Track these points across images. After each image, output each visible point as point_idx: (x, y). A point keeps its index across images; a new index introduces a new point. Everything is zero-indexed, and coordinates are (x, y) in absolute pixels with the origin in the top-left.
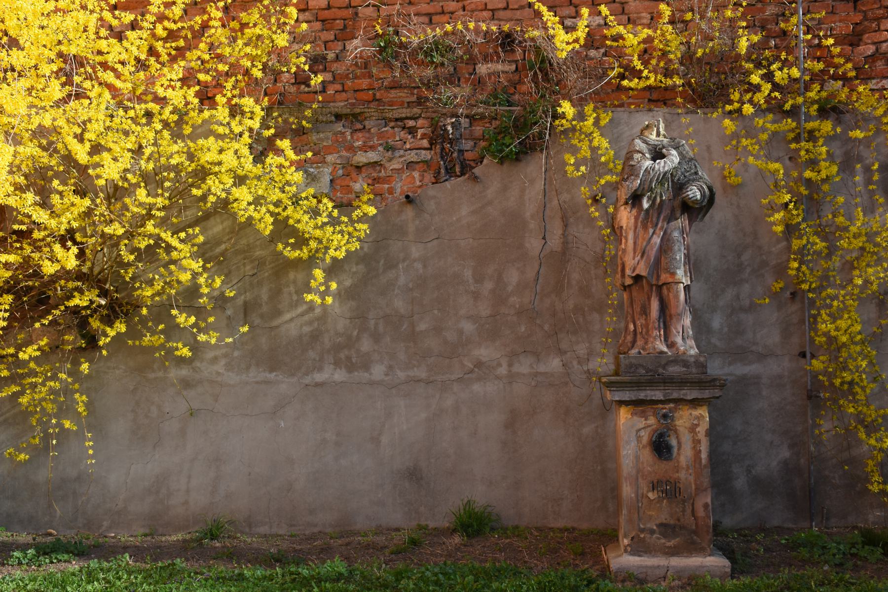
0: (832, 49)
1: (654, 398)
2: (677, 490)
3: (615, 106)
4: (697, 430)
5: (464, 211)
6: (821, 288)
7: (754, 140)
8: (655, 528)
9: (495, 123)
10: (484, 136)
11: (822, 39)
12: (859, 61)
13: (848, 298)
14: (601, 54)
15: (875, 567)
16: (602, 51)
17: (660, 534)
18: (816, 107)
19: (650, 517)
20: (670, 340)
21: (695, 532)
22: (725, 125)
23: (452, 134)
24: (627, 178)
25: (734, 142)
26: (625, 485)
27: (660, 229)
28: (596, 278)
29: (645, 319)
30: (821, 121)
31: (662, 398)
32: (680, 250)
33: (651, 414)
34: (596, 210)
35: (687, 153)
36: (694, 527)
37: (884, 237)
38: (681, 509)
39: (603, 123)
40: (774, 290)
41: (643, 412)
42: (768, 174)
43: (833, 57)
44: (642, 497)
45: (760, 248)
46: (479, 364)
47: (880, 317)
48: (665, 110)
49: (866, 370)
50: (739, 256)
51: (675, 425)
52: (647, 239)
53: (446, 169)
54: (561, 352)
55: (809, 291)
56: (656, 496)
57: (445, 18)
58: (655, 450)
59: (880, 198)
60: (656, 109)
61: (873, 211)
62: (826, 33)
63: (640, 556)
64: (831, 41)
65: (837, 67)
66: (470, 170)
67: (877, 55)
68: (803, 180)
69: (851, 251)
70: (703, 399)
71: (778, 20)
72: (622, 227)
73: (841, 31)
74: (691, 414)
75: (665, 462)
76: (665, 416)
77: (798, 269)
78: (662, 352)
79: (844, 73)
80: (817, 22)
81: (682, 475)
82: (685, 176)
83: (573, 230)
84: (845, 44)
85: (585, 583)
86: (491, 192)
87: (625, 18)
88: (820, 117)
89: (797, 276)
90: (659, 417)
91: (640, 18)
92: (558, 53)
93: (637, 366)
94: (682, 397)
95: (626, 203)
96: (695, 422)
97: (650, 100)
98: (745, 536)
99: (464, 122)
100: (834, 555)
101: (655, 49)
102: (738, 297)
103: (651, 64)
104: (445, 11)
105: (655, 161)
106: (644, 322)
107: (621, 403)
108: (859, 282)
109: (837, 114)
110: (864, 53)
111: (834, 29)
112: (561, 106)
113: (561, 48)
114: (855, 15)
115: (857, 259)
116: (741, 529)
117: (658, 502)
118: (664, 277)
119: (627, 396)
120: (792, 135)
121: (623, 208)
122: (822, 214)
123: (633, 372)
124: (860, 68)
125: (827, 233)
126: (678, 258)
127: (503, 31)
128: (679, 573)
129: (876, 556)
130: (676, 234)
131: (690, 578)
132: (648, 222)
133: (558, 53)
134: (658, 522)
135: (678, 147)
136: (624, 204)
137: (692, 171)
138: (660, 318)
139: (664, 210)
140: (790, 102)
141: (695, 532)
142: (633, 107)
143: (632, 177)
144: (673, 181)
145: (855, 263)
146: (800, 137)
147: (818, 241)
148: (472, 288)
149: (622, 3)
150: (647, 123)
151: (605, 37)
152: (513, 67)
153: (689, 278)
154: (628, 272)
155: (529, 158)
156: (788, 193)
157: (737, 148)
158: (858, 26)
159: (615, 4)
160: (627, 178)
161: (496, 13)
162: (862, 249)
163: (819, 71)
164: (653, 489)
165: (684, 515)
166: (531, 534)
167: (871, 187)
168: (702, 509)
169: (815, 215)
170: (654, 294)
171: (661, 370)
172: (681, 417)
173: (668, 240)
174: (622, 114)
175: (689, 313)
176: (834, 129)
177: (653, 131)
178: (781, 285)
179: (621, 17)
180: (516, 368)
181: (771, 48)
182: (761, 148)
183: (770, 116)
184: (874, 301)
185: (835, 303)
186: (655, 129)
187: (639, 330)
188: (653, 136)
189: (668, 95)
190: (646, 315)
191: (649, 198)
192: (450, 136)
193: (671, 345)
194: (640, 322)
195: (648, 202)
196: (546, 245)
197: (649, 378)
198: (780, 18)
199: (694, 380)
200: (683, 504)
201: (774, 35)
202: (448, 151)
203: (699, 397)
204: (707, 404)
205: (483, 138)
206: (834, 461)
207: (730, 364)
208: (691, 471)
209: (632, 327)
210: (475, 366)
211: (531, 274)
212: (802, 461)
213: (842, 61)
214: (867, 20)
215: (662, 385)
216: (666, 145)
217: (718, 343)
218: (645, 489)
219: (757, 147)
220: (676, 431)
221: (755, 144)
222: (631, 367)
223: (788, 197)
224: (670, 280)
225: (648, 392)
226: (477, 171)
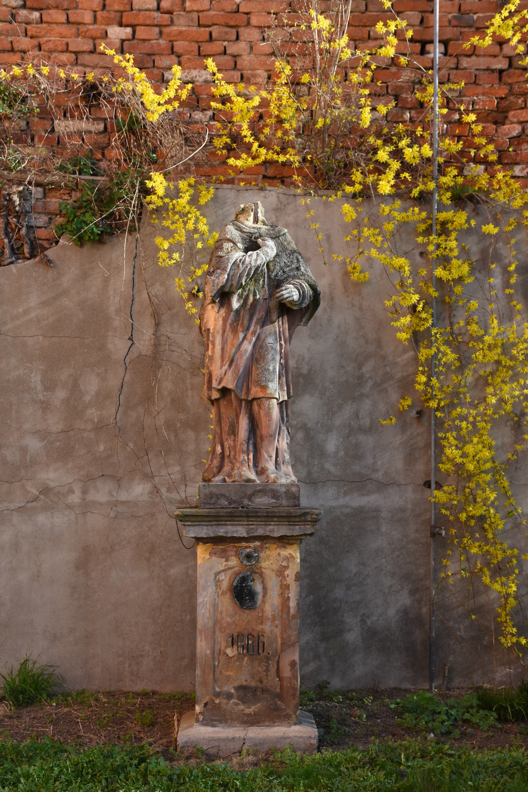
0: (473, 126)
1: (235, 535)
2: (261, 645)
3: (222, 183)
4: (286, 573)
5: (34, 301)
6: (452, 406)
7: (377, 231)
8: (233, 691)
9: (76, 195)
10: (61, 211)
11: (462, 114)
12: (503, 143)
13: (479, 419)
14: (208, 117)
15: (485, 735)
16: (210, 113)
17: (238, 699)
18: (449, 194)
19: (228, 678)
20: (260, 466)
21: (280, 696)
22: (344, 211)
23: (19, 205)
24: (213, 272)
25: (355, 232)
26: (199, 639)
27: (252, 334)
28: (192, 389)
29: (234, 440)
30: (455, 212)
31: (245, 535)
32: (274, 359)
33: (233, 553)
34: (194, 306)
35: (289, 243)
36: (278, 690)
37: (521, 350)
38: (264, 668)
39: (203, 201)
40: (401, 409)
41: (224, 551)
42: (392, 270)
43: (474, 136)
44: (219, 654)
45: (384, 358)
46: (46, 490)
47: (515, 442)
48: (281, 189)
49: (496, 503)
50: (360, 367)
51: (261, 567)
52: (236, 345)
53: (12, 248)
54: (148, 477)
55: (437, 409)
56: (236, 652)
57: (16, 58)
58: (236, 597)
59: (517, 304)
60: (268, 188)
61: (511, 319)
62: (468, 107)
63: (213, 726)
64: (472, 117)
65: (478, 148)
66: (42, 252)
67: (523, 137)
68: (434, 279)
69: (485, 365)
70: (293, 536)
71: (414, 89)
72: (209, 330)
73: (484, 106)
74: (279, 554)
75: (247, 611)
76: (249, 557)
77: (427, 384)
78: (249, 480)
79: (486, 156)
80: (457, 94)
81: (267, 627)
82: (284, 272)
83: (166, 329)
84: (488, 122)
85: (136, 762)
86: (66, 281)
87: (237, 75)
88: (456, 206)
89: (425, 392)
90: (241, 558)
91: (255, 76)
92: (149, 114)
93: (219, 496)
94: (268, 534)
95: (213, 302)
96: (284, 564)
97: (265, 177)
98: (351, 699)
99: (37, 192)
100: (443, 722)
101: (270, 116)
102: (356, 415)
103: (263, 133)
104: (16, 49)
105: (246, 253)
106: (232, 443)
107: (199, 540)
108: (493, 400)
109: (474, 204)
110: (508, 134)
111: (477, 104)
112: (150, 179)
113: (152, 109)
114: (499, 88)
115: (492, 374)
116: (349, 691)
117: (237, 660)
118: (255, 392)
119: (204, 532)
120: (422, 227)
121: (210, 307)
122: (454, 320)
123: (213, 504)
124: (504, 151)
125: (459, 342)
126: (271, 368)
127: (87, 81)
128: (257, 744)
129: (488, 722)
130: (270, 340)
131: (270, 752)
132: (238, 325)
133: (149, 114)
134: (236, 684)
135: (278, 237)
136: (211, 303)
137: (293, 266)
138: (249, 439)
139: (257, 312)
140: (421, 187)
141: (280, 696)
142: (242, 184)
143: (219, 271)
144: (269, 277)
145: (490, 378)
146: (432, 229)
147: (448, 351)
148: (41, 397)
149: (235, 56)
150: (242, 206)
151: (213, 97)
152: (101, 127)
153: (285, 393)
154: (215, 384)
155: (115, 240)
156: (416, 292)
157: (359, 240)
158: (503, 101)
159: (225, 57)
160: (213, 272)
161: (80, 57)
162: (498, 362)
163: (457, 152)
164: (233, 645)
165: (267, 675)
166: (97, 700)
167: (507, 291)
168: (289, 668)
169: (447, 321)
170: (243, 411)
171: (246, 502)
172: (268, 557)
173: (261, 347)
174: (228, 192)
175: (286, 432)
176: (468, 221)
177: (249, 216)
178: (409, 402)
179: (232, 73)
180: (93, 496)
181: (406, 121)
182: (385, 239)
183: (398, 203)
184: (508, 423)
186: (252, 214)
187: (227, 453)
188: (250, 223)
189: (285, 172)
190: (235, 436)
191: (240, 297)
192: (17, 209)
193: (261, 472)
195: (238, 300)
196: (134, 346)
197: (230, 510)
198: (417, 86)
199: (282, 514)
200: (267, 662)
201: (409, 106)
202: (14, 226)
203: (288, 534)
204: (298, 542)
205: (60, 214)
206: (460, 610)
207: (346, 494)
208: (277, 622)
209: (219, 449)
210: (40, 493)
211: (114, 382)
212: (424, 610)
213: (484, 141)
214: (513, 95)
215: (245, 519)
216: (263, 234)
217: (332, 469)
218: (223, 644)
219: (380, 238)
220: (261, 575)
221: (378, 235)
222: (211, 498)
223: (415, 298)
224: (261, 395)
225: (229, 527)
226: (51, 253)
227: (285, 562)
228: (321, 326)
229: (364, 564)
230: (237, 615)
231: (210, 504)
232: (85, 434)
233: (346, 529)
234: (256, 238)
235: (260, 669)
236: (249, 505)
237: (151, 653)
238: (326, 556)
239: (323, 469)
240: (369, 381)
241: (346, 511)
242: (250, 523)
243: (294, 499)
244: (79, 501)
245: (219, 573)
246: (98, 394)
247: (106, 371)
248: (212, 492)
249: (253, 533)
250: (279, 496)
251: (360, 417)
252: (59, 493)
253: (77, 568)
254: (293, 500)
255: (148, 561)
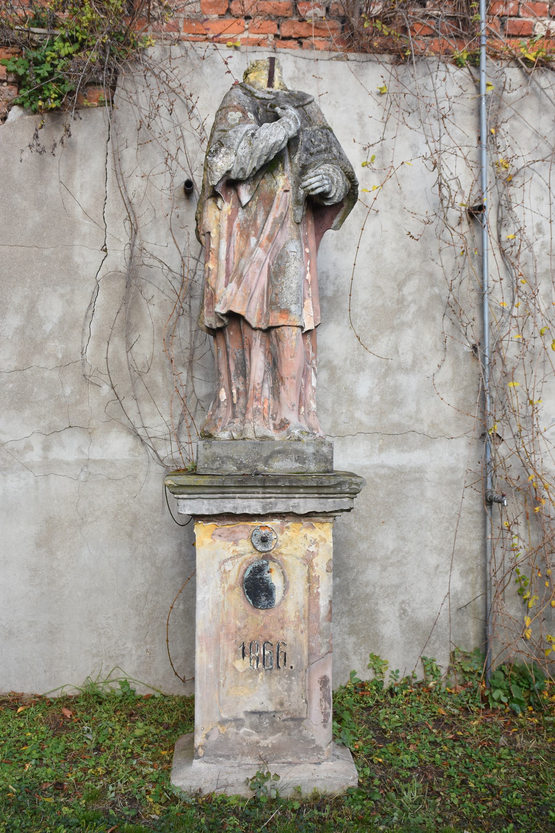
17: (251, 728)
24: (216, 151)
33: (246, 536)
38: (286, 686)
50: (400, 286)
74: (305, 536)
78: (264, 438)
94: (291, 510)
96: (313, 549)
123: (217, 469)
164: (244, 656)
165: (289, 696)
171: (261, 467)
180: (57, 453)
185: (147, 521)
194: (238, 384)
200: (289, 678)
203: (318, 511)
207: (381, 450)
215: (260, 490)
217: (365, 419)
218: (231, 655)
222: (214, 461)
225: (239, 501)
227: (313, 546)
228: (351, 233)
229: (403, 539)
230: (250, 618)
231: (212, 469)
232: (46, 374)
233: (381, 495)
234: (273, 106)
235: (280, 688)
236: (265, 471)
237: (134, 652)
238: (356, 529)
239: (352, 418)
240: (412, 305)
241: (383, 471)
242: (268, 495)
243: (326, 462)
244: (40, 460)
245: (226, 561)
246: (62, 322)
247: (72, 291)
248: (215, 453)
249: (271, 508)
250: (305, 459)
251: (400, 352)
252: (13, 449)
253: (38, 545)
254: (323, 464)
255: (130, 536)
